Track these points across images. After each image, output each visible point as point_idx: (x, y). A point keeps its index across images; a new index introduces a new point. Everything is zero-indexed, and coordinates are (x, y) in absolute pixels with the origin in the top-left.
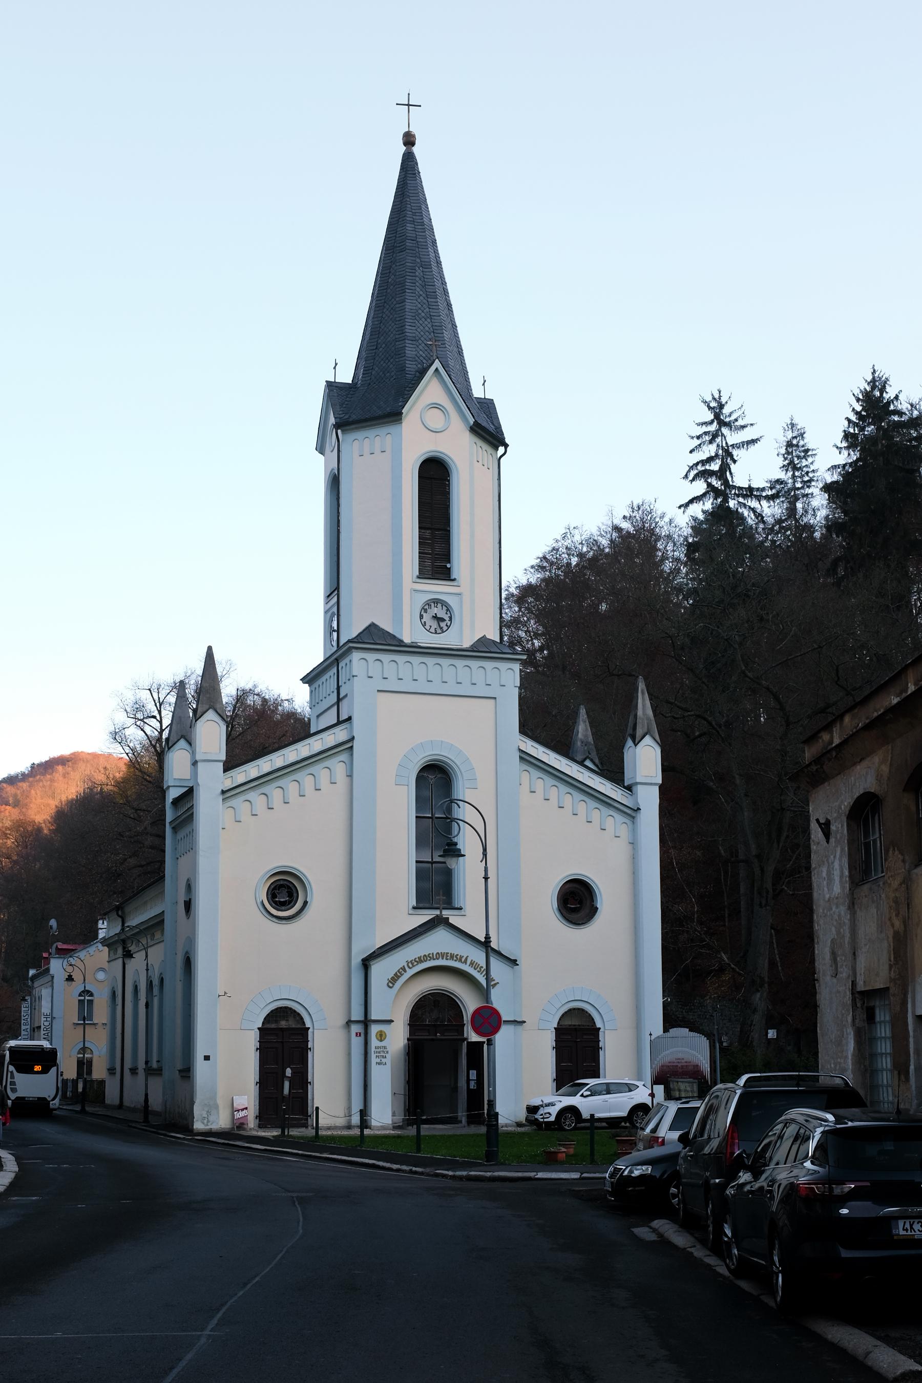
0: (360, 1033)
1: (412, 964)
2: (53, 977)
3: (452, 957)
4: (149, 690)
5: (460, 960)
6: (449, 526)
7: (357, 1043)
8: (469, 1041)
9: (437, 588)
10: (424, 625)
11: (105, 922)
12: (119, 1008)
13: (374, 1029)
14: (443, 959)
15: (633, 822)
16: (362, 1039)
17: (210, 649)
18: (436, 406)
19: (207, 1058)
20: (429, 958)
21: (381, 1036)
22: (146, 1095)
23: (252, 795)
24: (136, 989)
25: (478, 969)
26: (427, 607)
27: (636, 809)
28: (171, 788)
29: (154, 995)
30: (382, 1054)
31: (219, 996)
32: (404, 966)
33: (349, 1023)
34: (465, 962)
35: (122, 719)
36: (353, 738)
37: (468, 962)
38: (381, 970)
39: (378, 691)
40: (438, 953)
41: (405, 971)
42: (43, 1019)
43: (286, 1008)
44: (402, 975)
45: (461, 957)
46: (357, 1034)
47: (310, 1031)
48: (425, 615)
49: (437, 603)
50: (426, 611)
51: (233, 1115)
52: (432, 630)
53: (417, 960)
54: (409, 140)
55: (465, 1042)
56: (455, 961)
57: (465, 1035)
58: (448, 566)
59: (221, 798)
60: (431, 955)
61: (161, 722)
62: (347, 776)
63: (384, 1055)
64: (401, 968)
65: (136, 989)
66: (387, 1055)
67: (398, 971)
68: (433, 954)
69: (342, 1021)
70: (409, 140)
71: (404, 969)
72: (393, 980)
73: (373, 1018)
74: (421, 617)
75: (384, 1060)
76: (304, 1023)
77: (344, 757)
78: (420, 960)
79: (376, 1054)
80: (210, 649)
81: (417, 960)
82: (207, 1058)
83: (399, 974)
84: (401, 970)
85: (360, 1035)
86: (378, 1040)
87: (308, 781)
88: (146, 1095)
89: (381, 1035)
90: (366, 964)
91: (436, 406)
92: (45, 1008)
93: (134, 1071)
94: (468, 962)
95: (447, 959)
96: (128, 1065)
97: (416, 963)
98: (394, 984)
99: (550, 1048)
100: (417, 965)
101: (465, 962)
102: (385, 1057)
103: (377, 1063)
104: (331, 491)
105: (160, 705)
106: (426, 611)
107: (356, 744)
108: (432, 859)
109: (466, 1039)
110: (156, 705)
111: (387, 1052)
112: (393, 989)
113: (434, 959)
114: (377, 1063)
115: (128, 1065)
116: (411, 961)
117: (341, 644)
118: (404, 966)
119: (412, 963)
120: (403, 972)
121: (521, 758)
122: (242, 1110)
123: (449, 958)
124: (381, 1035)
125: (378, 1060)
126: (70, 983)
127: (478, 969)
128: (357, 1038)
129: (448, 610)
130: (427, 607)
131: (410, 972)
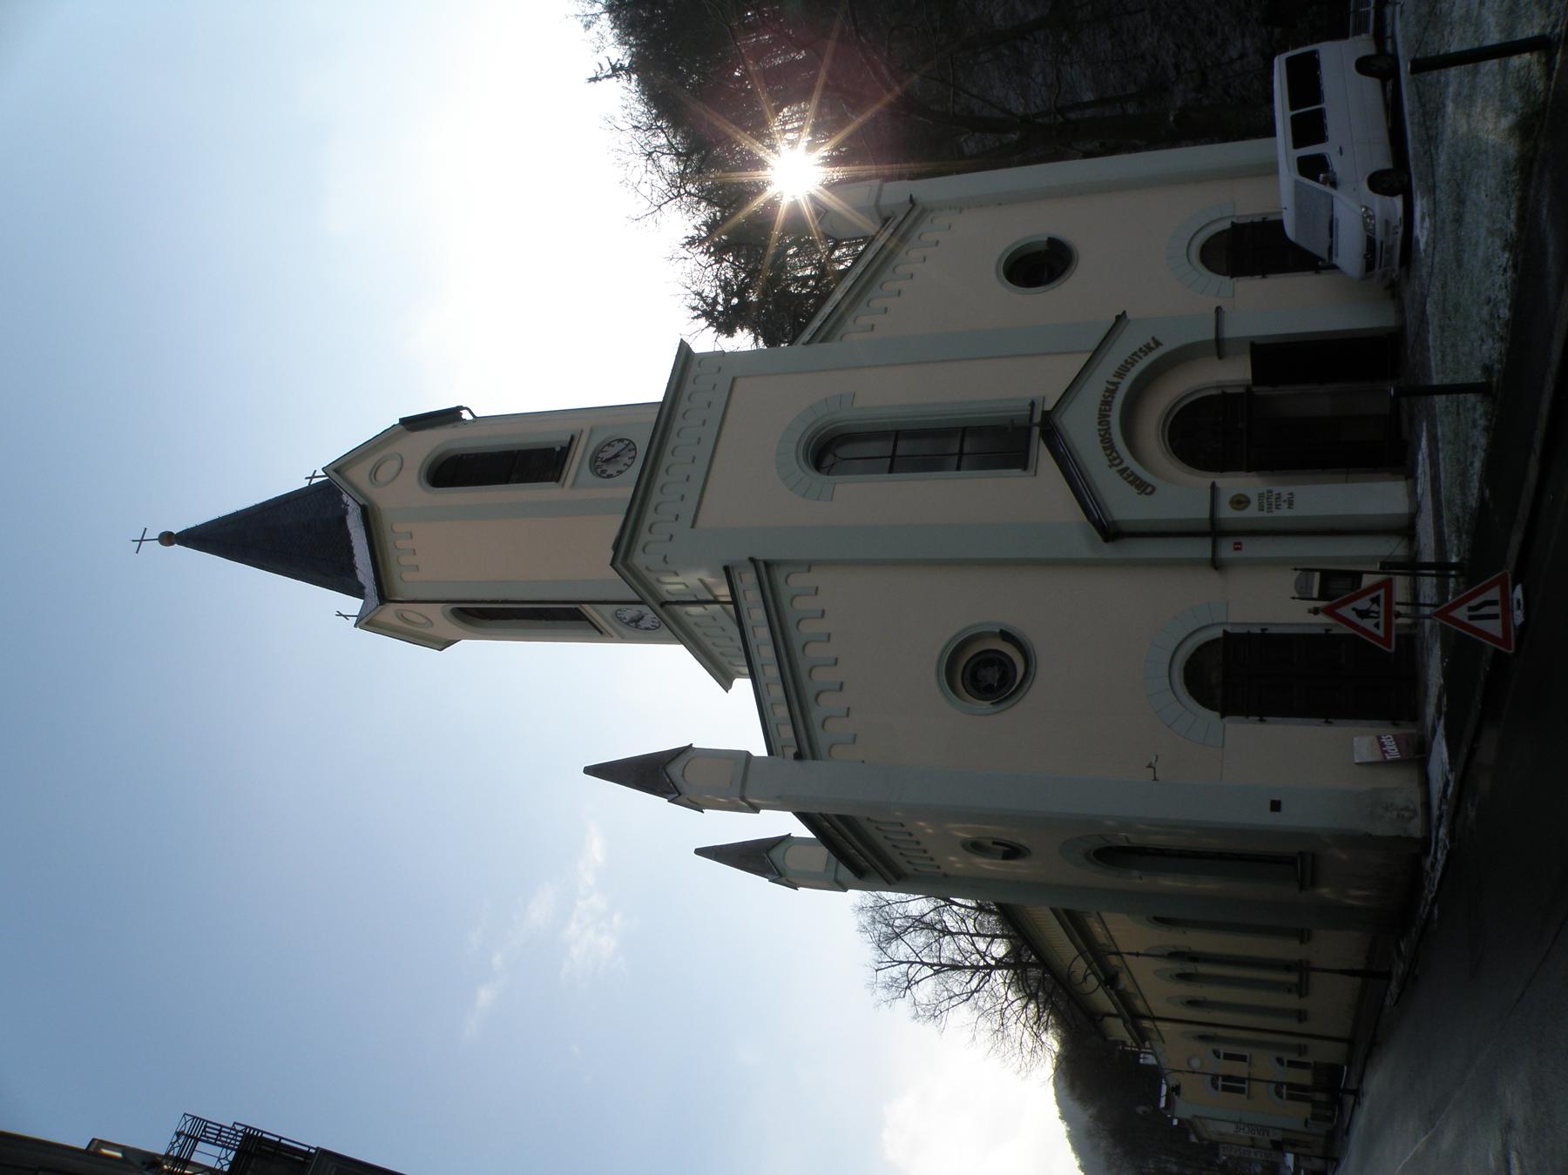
0: (1236, 544)
1: (1115, 459)
2: (1195, 1116)
3: (1107, 403)
4: (877, 971)
5: (1114, 391)
6: (512, 452)
7: (1255, 548)
8: (1251, 382)
9: (577, 462)
10: (620, 472)
11: (1032, 1006)
12: (1220, 1032)
14: (1109, 416)
15: (932, 211)
16: (1247, 542)
19: (1276, 806)
20: (1107, 436)
21: (1240, 502)
22: (1342, 972)
23: (816, 715)
24: (1193, 1003)
25: (1129, 366)
26: (599, 471)
27: (911, 205)
28: (838, 878)
29: (1193, 971)
30: (1273, 500)
31: (1155, 779)
32: (1118, 471)
33: (1216, 564)
35: (903, 1006)
36: (752, 560)
37: (1116, 380)
38: (1123, 505)
39: (693, 526)
40: (1100, 423)
41: (1126, 469)
42: (1241, 1133)
43: (1186, 670)
44: (1133, 473)
45: (1107, 390)
46: (1236, 549)
47: (1229, 629)
48: (607, 473)
49: (597, 458)
50: (604, 472)
51: (1394, 762)
52: (629, 462)
53: (1107, 394)
54: (167, 539)
55: (1255, 389)
56: (1113, 397)
57: (1241, 390)
58: (558, 449)
59: (809, 763)
60: (1102, 433)
61: (912, 963)
62: (809, 570)
63: (1274, 497)
64: (1121, 475)
65: (1193, 1003)
66: (1274, 493)
67: (1126, 479)
68: (1100, 430)
69: (1213, 577)
70: (167, 539)
71: (1122, 472)
72: (1142, 487)
73: (1206, 514)
74: (610, 476)
75: (1285, 497)
76: (1215, 641)
77: (779, 575)
79: (1274, 509)
81: (1108, 452)
83: (1131, 478)
84: (1125, 475)
85: (1240, 544)
86: (1247, 506)
87: (808, 628)
88: (1342, 972)
89: (1239, 502)
90: (1110, 532)
92: (1229, 1128)
93: (1301, 1016)
94: (1116, 380)
95: (1110, 410)
96: (1292, 1024)
97: (1114, 454)
98: (1149, 485)
99: (1265, 281)
100: (1117, 452)
101: (1116, 384)
102: (1279, 494)
103: (1289, 508)
104: (471, 624)
105: (894, 961)
107: (760, 556)
108: (955, 454)
109: (1248, 389)
110: (893, 966)
111: (1270, 492)
112: (1154, 484)
113: (1109, 428)
114: (1289, 508)
115: (1292, 1024)
116: (1110, 461)
117: (636, 598)
118: (1118, 471)
120: (1129, 472)
122: (1382, 745)
123: (1107, 408)
124: (1239, 502)
125: (1285, 506)
126: (1182, 1091)
127: (1129, 366)
128: (1244, 547)
129: (609, 445)
130: (599, 471)
131: (1129, 461)
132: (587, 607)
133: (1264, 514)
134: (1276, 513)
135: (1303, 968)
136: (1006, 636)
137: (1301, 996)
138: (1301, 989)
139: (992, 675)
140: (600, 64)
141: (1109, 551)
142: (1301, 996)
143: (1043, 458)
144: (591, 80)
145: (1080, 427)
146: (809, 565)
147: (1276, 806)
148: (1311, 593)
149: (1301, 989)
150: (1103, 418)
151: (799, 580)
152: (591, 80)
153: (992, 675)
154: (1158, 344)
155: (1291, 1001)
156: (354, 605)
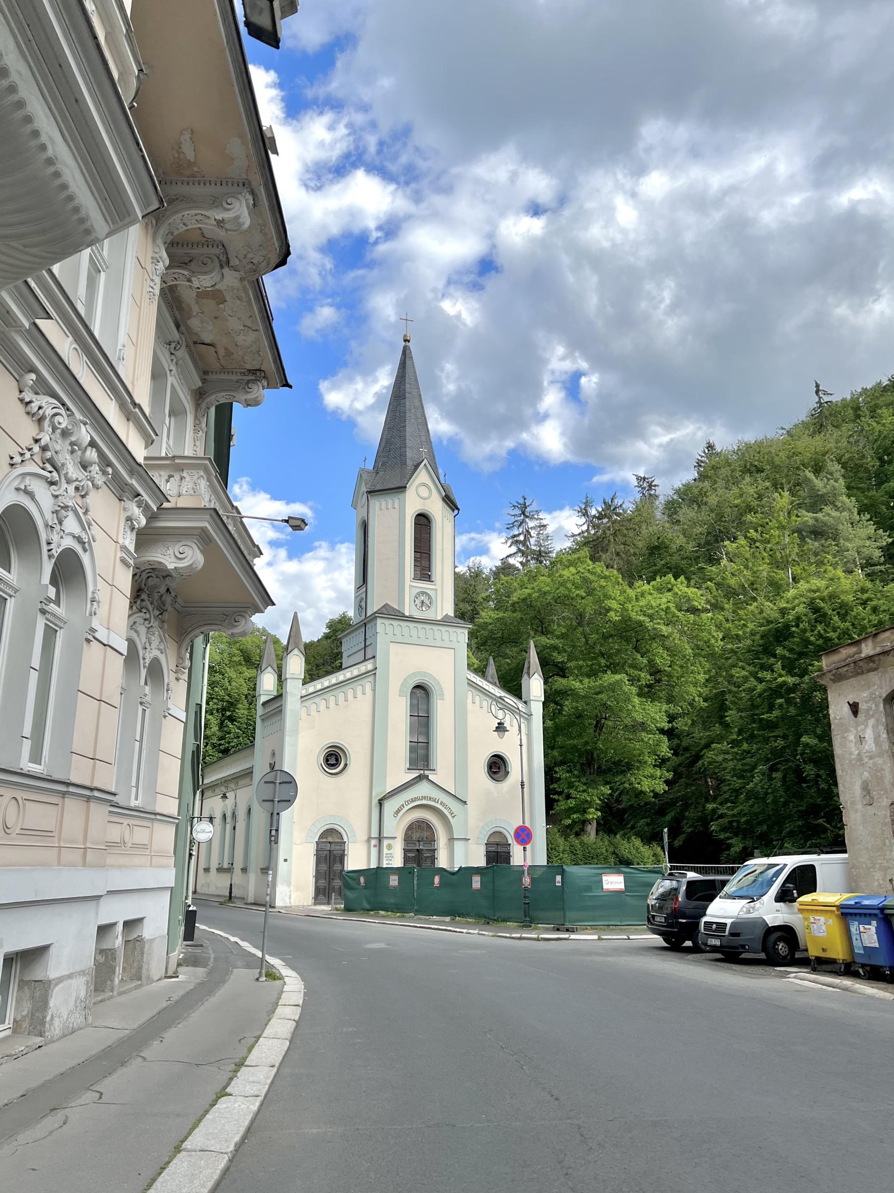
7: (374, 851)
9: (423, 585)
13: (386, 843)
17: (296, 613)
18: (424, 485)
21: (389, 847)
23: (317, 700)
33: (370, 839)
34: (438, 802)
38: (390, 806)
69: (366, 838)
71: (430, 798)
74: (415, 601)
77: (371, 679)
78: (413, 801)
80: (296, 613)
82: (286, 860)
90: (381, 802)
91: (424, 485)
93: (207, 870)
99: (313, 855)
106: (417, 598)
117: (368, 615)
119: (408, 802)
121: (468, 683)
131: (407, 808)
132: (365, 589)
133: (385, 855)
134: (385, 859)
135: (229, 870)
136: (346, 765)
137: (217, 869)
138: (220, 870)
139: (332, 761)
140: (831, 394)
141: (375, 801)
142: (217, 869)
143: (414, 774)
144: (817, 386)
145: (423, 790)
146: (374, 690)
147: (824, 950)
148: (153, 792)
149: (220, 870)
150: (424, 798)
151: (368, 688)
152: (817, 386)
153: (332, 761)
154: (453, 817)
155: (214, 866)
156: (370, 466)
